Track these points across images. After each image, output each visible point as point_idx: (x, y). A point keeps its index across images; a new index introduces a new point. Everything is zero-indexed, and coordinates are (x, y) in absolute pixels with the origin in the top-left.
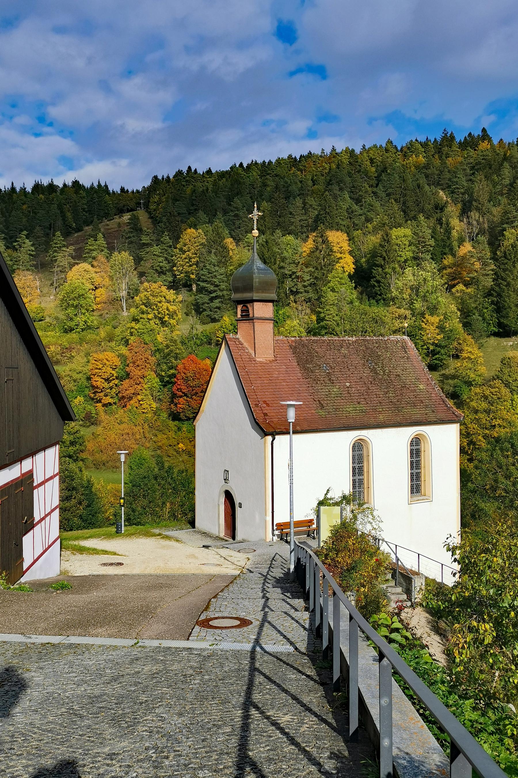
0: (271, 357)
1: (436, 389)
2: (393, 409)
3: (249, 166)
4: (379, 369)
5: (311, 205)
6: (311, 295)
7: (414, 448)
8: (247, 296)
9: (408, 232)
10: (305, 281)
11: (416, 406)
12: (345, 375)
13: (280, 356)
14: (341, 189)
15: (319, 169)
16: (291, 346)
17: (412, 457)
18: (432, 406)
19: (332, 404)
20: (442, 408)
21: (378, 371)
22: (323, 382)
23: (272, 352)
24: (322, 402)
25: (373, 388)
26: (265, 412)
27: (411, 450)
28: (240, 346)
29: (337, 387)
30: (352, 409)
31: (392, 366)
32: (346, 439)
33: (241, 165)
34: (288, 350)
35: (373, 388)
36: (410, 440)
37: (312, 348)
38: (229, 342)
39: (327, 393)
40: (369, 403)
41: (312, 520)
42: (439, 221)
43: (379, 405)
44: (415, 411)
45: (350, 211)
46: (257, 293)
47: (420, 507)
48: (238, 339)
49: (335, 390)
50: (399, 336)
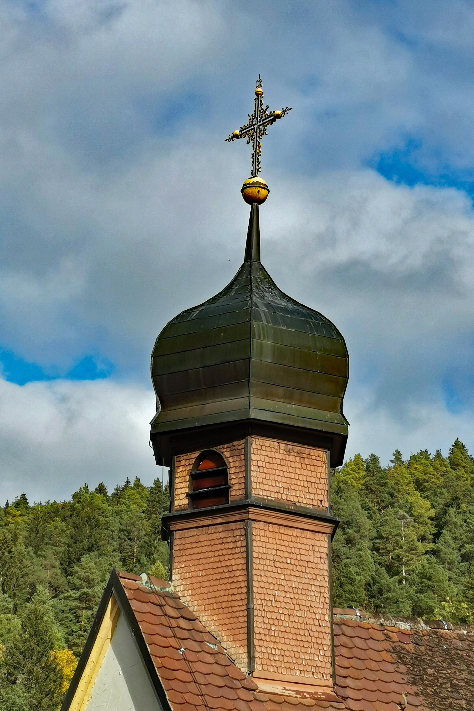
3: (119, 494)
13: (359, 684)
16: (399, 654)
23: (322, 658)
28: (183, 623)
33: (101, 489)
34: (391, 668)
38: (134, 605)
45: (375, 588)
46: (267, 395)
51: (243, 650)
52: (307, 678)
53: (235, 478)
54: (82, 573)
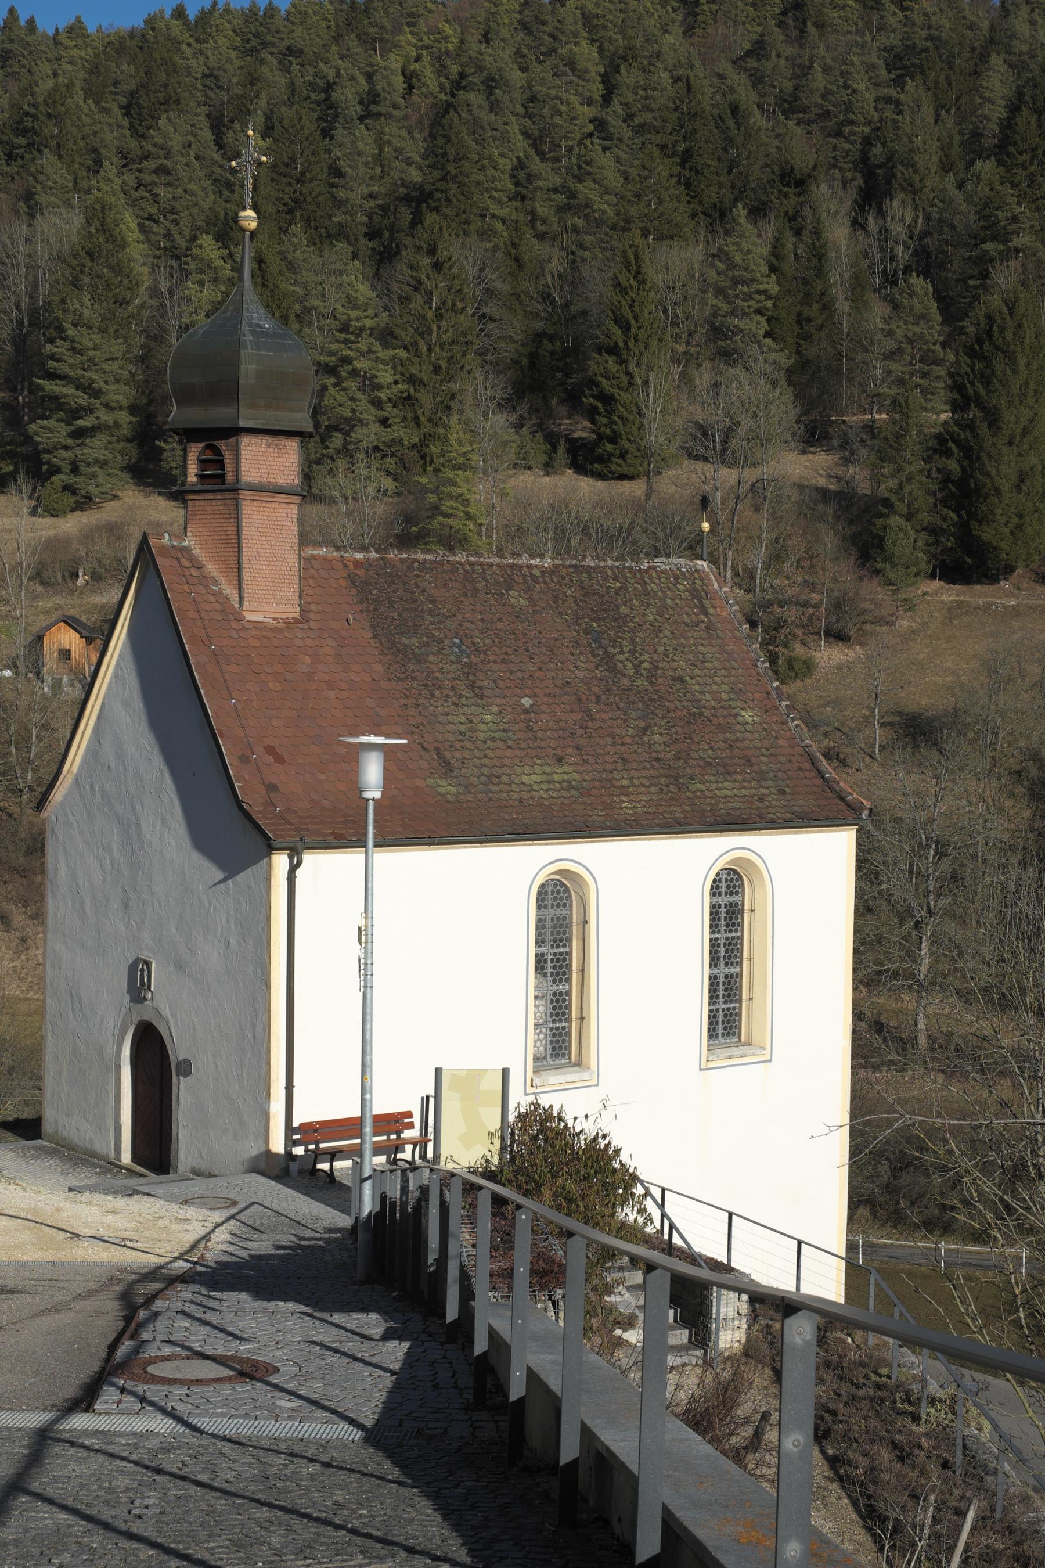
0: (292, 611)
1: (792, 725)
2: (662, 780)
4: (622, 657)
5: (399, 151)
6: (398, 431)
7: (723, 900)
8: (216, 415)
9: (696, 254)
10: (380, 387)
11: (730, 774)
12: (520, 675)
14: (494, 106)
15: (425, 38)
16: (352, 579)
17: (714, 927)
18: (780, 774)
19: (477, 762)
20: (807, 782)
21: (620, 665)
22: (452, 694)
24: (448, 755)
25: (605, 716)
26: (271, 779)
27: (713, 906)
28: (194, 572)
29: (495, 709)
30: (538, 778)
31: (661, 649)
32: (518, 867)
33: (179, 13)
35: (605, 716)
36: (712, 876)
37: (416, 585)
39: (463, 728)
40: (591, 760)
41: (409, 1114)
42: (794, 222)
43: (620, 766)
44: (728, 789)
47: (736, 1077)
48: (187, 550)
49: (488, 718)
50: (682, 561)
51: (235, 592)
52: (281, 608)
53: (229, 468)
54: (159, 140)
